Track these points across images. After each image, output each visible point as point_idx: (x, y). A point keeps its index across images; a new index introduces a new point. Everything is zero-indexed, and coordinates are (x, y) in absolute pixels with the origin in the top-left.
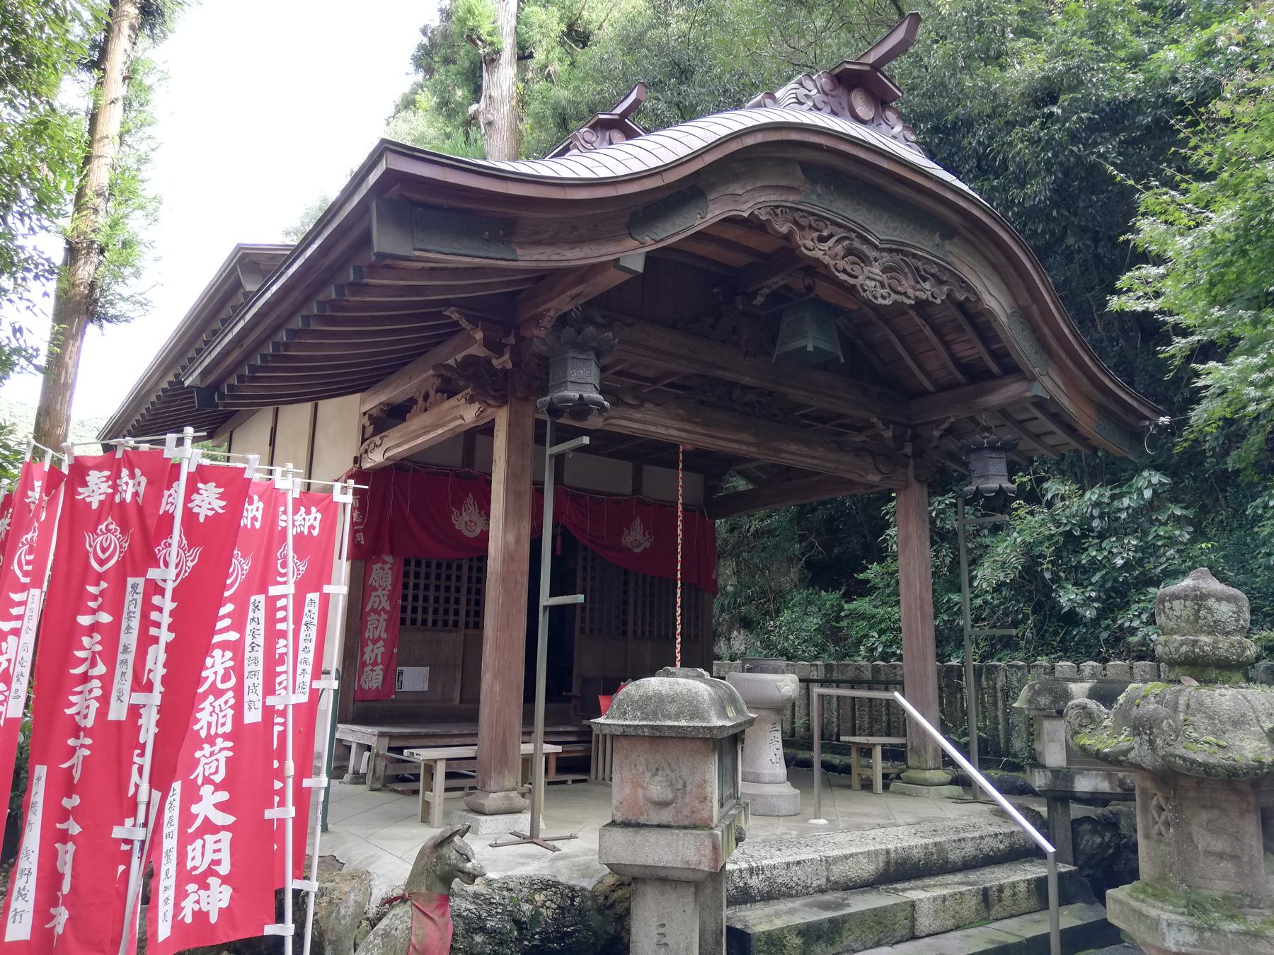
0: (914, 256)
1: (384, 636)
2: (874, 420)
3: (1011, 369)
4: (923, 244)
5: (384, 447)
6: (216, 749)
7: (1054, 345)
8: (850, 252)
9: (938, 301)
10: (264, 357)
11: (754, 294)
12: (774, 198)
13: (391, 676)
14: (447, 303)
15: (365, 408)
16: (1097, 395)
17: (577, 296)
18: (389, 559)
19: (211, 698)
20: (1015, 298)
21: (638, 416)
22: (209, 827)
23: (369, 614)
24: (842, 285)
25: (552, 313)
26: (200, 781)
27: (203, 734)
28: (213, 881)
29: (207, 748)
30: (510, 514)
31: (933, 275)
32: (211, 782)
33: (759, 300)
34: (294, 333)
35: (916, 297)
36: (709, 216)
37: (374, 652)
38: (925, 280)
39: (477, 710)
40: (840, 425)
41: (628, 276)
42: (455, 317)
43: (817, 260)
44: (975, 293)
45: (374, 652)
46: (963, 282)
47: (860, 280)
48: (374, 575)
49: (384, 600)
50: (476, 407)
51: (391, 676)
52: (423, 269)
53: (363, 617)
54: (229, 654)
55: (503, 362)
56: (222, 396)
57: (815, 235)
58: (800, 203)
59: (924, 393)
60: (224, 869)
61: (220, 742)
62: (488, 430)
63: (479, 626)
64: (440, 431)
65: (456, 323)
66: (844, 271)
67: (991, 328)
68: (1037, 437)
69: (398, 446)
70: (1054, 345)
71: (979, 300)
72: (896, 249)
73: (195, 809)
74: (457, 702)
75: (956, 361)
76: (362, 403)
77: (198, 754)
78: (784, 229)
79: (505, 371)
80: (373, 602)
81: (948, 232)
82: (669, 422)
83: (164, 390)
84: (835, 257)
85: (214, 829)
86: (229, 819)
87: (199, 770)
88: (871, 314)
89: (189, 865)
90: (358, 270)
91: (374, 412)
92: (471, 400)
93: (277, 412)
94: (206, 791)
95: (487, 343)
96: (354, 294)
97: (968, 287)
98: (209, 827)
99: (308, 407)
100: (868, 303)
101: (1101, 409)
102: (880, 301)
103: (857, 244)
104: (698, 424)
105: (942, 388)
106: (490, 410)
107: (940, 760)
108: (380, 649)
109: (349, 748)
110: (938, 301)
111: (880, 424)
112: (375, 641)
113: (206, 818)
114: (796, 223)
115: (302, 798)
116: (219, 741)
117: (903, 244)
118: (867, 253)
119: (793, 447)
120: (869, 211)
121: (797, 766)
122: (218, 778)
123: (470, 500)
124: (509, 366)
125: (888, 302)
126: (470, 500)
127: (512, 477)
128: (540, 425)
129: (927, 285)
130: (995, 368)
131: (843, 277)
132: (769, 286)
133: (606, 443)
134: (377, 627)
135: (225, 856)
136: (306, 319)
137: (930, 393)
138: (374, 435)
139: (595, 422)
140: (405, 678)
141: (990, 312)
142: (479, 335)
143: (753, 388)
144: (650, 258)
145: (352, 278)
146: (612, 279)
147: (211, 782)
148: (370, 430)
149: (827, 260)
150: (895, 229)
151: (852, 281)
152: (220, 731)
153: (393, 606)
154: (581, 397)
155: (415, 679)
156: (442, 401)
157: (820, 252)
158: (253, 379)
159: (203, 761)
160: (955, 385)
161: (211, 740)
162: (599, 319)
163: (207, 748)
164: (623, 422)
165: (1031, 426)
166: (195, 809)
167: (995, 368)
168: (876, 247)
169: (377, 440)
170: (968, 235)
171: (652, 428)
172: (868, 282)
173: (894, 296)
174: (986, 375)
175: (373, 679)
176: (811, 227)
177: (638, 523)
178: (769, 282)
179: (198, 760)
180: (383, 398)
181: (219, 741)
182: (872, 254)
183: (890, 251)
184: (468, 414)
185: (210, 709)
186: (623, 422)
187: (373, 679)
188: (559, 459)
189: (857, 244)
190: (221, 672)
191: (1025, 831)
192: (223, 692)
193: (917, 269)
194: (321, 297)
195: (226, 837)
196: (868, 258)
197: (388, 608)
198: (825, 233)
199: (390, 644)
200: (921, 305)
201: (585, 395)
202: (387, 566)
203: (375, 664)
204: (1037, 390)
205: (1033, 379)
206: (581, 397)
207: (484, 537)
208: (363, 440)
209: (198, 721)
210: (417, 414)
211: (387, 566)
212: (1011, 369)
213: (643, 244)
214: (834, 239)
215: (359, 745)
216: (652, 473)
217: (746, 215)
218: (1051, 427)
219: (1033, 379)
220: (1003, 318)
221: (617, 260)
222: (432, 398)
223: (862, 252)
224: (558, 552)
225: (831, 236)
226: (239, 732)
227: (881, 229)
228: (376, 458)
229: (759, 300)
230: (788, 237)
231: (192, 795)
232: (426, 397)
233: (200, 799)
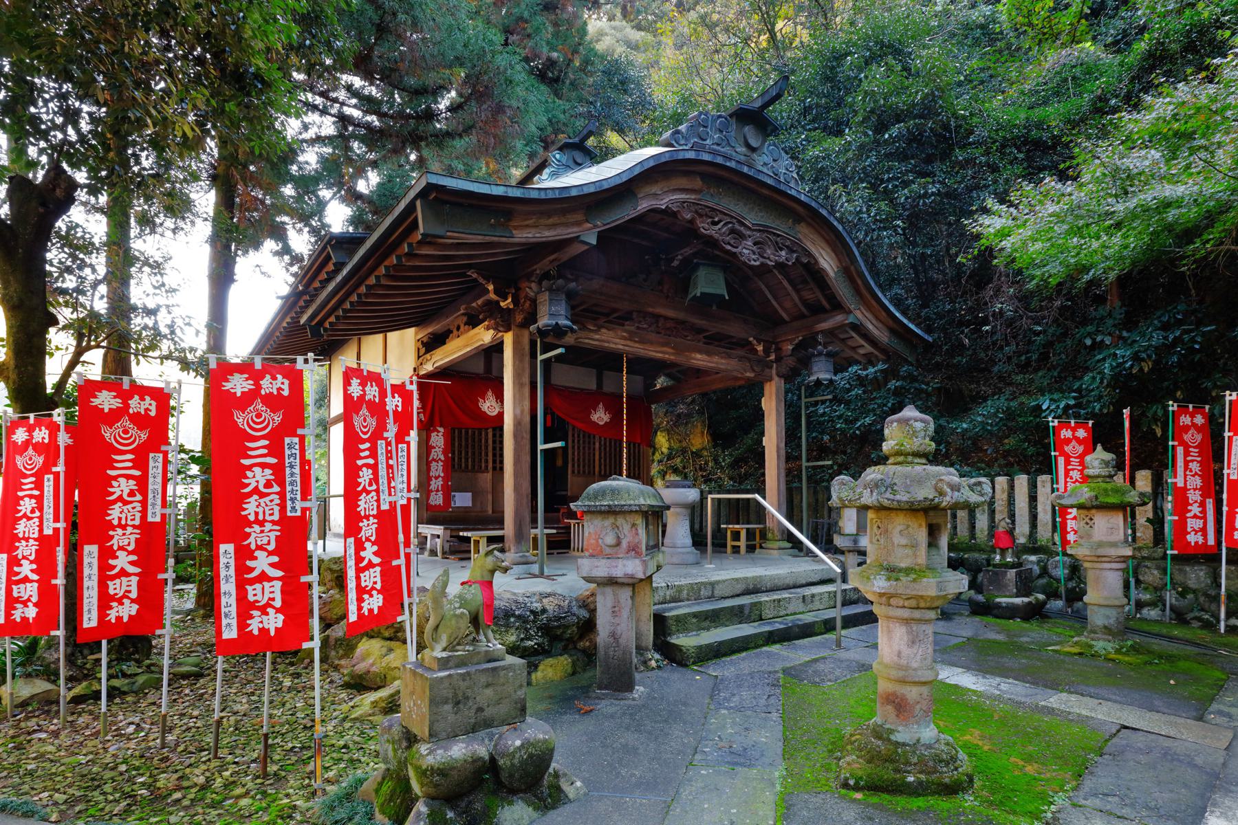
0: (774, 234)
1: (442, 475)
2: (751, 339)
3: (837, 306)
4: (781, 226)
5: (433, 361)
6: (370, 522)
7: (864, 291)
8: (733, 231)
9: (790, 263)
10: (351, 303)
11: (673, 260)
12: (683, 196)
13: (448, 498)
14: (469, 266)
15: (419, 337)
16: (891, 322)
17: (553, 260)
18: (441, 430)
19: (364, 494)
20: (839, 260)
21: (597, 337)
22: (371, 565)
23: (431, 462)
24: (728, 252)
25: (538, 272)
26: (364, 539)
27: (363, 514)
28: (374, 592)
29: (365, 522)
30: (517, 399)
31: (787, 247)
32: (370, 541)
33: (676, 263)
34: (369, 287)
35: (776, 261)
36: (639, 208)
37: (436, 484)
38: (781, 249)
39: (503, 517)
40: (729, 343)
41: (586, 247)
42: (475, 276)
43: (711, 237)
44: (814, 259)
45: (436, 484)
46: (807, 251)
47: (739, 250)
48: (432, 439)
49: (440, 453)
50: (491, 332)
51: (448, 498)
52: (452, 244)
53: (428, 464)
54: (370, 471)
55: (506, 304)
56: (325, 330)
57: (710, 220)
58: (699, 200)
59: (784, 322)
60: (378, 586)
61: (372, 520)
62: (498, 348)
63: (502, 469)
64: (468, 349)
65: (475, 280)
66: (729, 244)
67: (825, 281)
68: (854, 349)
69: (442, 359)
70: (864, 291)
71: (816, 262)
72: (764, 230)
73: (363, 554)
74: (490, 512)
75: (804, 302)
76: (416, 333)
77: (361, 524)
78: (689, 216)
79: (508, 310)
80: (433, 455)
81: (798, 219)
82: (618, 341)
83: (284, 328)
84: (721, 235)
85: (270, 579)
86: (280, 573)
87: (363, 533)
88: (750, 273)
89: (363, 584)
90: (410, 245)
91: (425, 340)
92: (488, 328)
93: (360, 339)
94: (367, 545)
95: (496, 292)
96: (408, 261)
97: (810, 255)
98: (371, 565)
99: (380, 337)
100: (745, 263)
101: (892, 331)
102: (753, 263)
103: (737, 226)
104: (636, 342)
105: (795, 319)
106: (500, 334)
107: (785, 536)
108: (440, 482)
109: (426, 537)
110: (790, 263)
111: (755, 342)
112: (436, 478)
113: (370, 560)
114: (696, 212)
115: (408, 556)
116: (371, 518)
117: (767, 227)
118: (744, 232)
119: (699, 356)
120: (745, 204)
121: (698, 541)
122: (272, 547)
123: (490, 393)
124: (511, 306)
125: (757, 263)
126: (490, 393)
127: (517, 375)
128: (533, 344)
129: (783, 253)
130: (827, 306)
131: (729, 247)
132: (682, 254)
133: (576, 356)
134: (437, 469)
135: (378, 579)
136: (378, 278)
137: (786, 322)
138: (425, 354)
139: (569, 339)
140: (457, 499)
141: (823, 270)
142: (491, 287)
143: (672, 319)
144: (601, 236)
145: (406, 250)
146: (578, 249)
147: (370, 541)
148: (423, 350)
149: (716, 236)
150: (762, 217)
151: (734, 250)
152: (371, 513)
153: (446, 456)
154: (557, 323)
155: (463, 500)
156: (469, 330)
157: (713, 231)
158: (346, 318)
159: (364, 528)
160: (802, 316)
161: (367, 517)
162: (570, 276)
163: (257, 528)
164: (587, 341)
165: (850, 343)
166: (363, 554)
167: (827, 306)
168: (750, 228)
169: (428, 356)
170: (809, 220)
171: (606, 345)
172: (744, 251)
173: (761, 259)
174: (825, 311)
175: (437, 499)
176: (707, 215)
177: (601, 406)
178: (682, 251)
179: (361, 528)
180: (430, 330)
181: (371, 518)
182: (749, 233)
183: (760, 231)
184: (484, 336)
185: (364, 500)
186: (587, 341)
187: (437, 499)
188: (546, 362)
189: (737, 226)
190: (368, 481)
191: (831, 568)
192: (370, 492)
193: (777, 242)
194: (387, 263)
195: (278, 584)
196: (744, 235)
197: (443, 458)
198: (716, 219)
199: (446, 479)
200: (780, 266)
201: (560, 322)
202: (440, 434)
203: (437, 491)
204: (851, 319)
205: (850, 312)
206: (557, 323)
207: (501, 415)
208: (419, 357)
209: (359, 506)
210: (453, 339)
211: (440, 434)
212: (837, 306)
213: (595, 226)
214: (722, 224)
215: (432, 535)
216: (609, 376)
217: (663, 207)
218: (863, 343)
219: (850, 312)
220: (832, 274)
221: (579, 236)
222: (462, 329)
223: (741, 232)
224: (549, 424)
225: (720, 221)
226: (380, 515)
227: (753, 217)
228: (429, 367)
229: (676, 263)
230: (692, 221)
231: (244, 554)
232: (458, 328)
233: (365, 549)
